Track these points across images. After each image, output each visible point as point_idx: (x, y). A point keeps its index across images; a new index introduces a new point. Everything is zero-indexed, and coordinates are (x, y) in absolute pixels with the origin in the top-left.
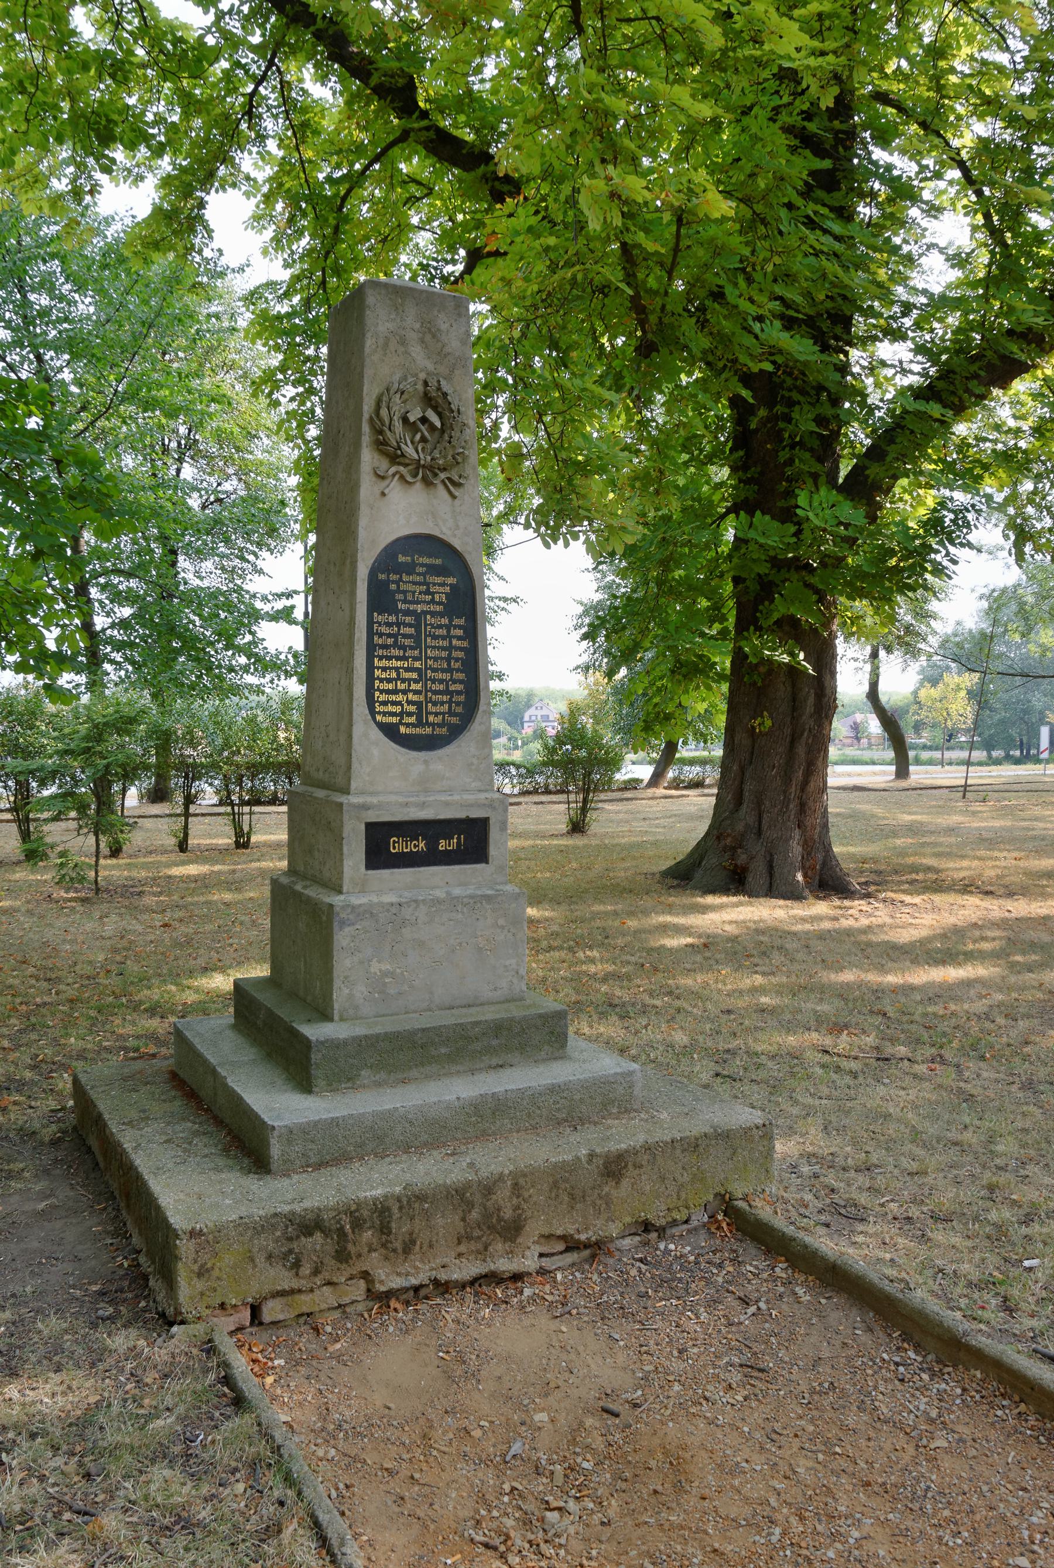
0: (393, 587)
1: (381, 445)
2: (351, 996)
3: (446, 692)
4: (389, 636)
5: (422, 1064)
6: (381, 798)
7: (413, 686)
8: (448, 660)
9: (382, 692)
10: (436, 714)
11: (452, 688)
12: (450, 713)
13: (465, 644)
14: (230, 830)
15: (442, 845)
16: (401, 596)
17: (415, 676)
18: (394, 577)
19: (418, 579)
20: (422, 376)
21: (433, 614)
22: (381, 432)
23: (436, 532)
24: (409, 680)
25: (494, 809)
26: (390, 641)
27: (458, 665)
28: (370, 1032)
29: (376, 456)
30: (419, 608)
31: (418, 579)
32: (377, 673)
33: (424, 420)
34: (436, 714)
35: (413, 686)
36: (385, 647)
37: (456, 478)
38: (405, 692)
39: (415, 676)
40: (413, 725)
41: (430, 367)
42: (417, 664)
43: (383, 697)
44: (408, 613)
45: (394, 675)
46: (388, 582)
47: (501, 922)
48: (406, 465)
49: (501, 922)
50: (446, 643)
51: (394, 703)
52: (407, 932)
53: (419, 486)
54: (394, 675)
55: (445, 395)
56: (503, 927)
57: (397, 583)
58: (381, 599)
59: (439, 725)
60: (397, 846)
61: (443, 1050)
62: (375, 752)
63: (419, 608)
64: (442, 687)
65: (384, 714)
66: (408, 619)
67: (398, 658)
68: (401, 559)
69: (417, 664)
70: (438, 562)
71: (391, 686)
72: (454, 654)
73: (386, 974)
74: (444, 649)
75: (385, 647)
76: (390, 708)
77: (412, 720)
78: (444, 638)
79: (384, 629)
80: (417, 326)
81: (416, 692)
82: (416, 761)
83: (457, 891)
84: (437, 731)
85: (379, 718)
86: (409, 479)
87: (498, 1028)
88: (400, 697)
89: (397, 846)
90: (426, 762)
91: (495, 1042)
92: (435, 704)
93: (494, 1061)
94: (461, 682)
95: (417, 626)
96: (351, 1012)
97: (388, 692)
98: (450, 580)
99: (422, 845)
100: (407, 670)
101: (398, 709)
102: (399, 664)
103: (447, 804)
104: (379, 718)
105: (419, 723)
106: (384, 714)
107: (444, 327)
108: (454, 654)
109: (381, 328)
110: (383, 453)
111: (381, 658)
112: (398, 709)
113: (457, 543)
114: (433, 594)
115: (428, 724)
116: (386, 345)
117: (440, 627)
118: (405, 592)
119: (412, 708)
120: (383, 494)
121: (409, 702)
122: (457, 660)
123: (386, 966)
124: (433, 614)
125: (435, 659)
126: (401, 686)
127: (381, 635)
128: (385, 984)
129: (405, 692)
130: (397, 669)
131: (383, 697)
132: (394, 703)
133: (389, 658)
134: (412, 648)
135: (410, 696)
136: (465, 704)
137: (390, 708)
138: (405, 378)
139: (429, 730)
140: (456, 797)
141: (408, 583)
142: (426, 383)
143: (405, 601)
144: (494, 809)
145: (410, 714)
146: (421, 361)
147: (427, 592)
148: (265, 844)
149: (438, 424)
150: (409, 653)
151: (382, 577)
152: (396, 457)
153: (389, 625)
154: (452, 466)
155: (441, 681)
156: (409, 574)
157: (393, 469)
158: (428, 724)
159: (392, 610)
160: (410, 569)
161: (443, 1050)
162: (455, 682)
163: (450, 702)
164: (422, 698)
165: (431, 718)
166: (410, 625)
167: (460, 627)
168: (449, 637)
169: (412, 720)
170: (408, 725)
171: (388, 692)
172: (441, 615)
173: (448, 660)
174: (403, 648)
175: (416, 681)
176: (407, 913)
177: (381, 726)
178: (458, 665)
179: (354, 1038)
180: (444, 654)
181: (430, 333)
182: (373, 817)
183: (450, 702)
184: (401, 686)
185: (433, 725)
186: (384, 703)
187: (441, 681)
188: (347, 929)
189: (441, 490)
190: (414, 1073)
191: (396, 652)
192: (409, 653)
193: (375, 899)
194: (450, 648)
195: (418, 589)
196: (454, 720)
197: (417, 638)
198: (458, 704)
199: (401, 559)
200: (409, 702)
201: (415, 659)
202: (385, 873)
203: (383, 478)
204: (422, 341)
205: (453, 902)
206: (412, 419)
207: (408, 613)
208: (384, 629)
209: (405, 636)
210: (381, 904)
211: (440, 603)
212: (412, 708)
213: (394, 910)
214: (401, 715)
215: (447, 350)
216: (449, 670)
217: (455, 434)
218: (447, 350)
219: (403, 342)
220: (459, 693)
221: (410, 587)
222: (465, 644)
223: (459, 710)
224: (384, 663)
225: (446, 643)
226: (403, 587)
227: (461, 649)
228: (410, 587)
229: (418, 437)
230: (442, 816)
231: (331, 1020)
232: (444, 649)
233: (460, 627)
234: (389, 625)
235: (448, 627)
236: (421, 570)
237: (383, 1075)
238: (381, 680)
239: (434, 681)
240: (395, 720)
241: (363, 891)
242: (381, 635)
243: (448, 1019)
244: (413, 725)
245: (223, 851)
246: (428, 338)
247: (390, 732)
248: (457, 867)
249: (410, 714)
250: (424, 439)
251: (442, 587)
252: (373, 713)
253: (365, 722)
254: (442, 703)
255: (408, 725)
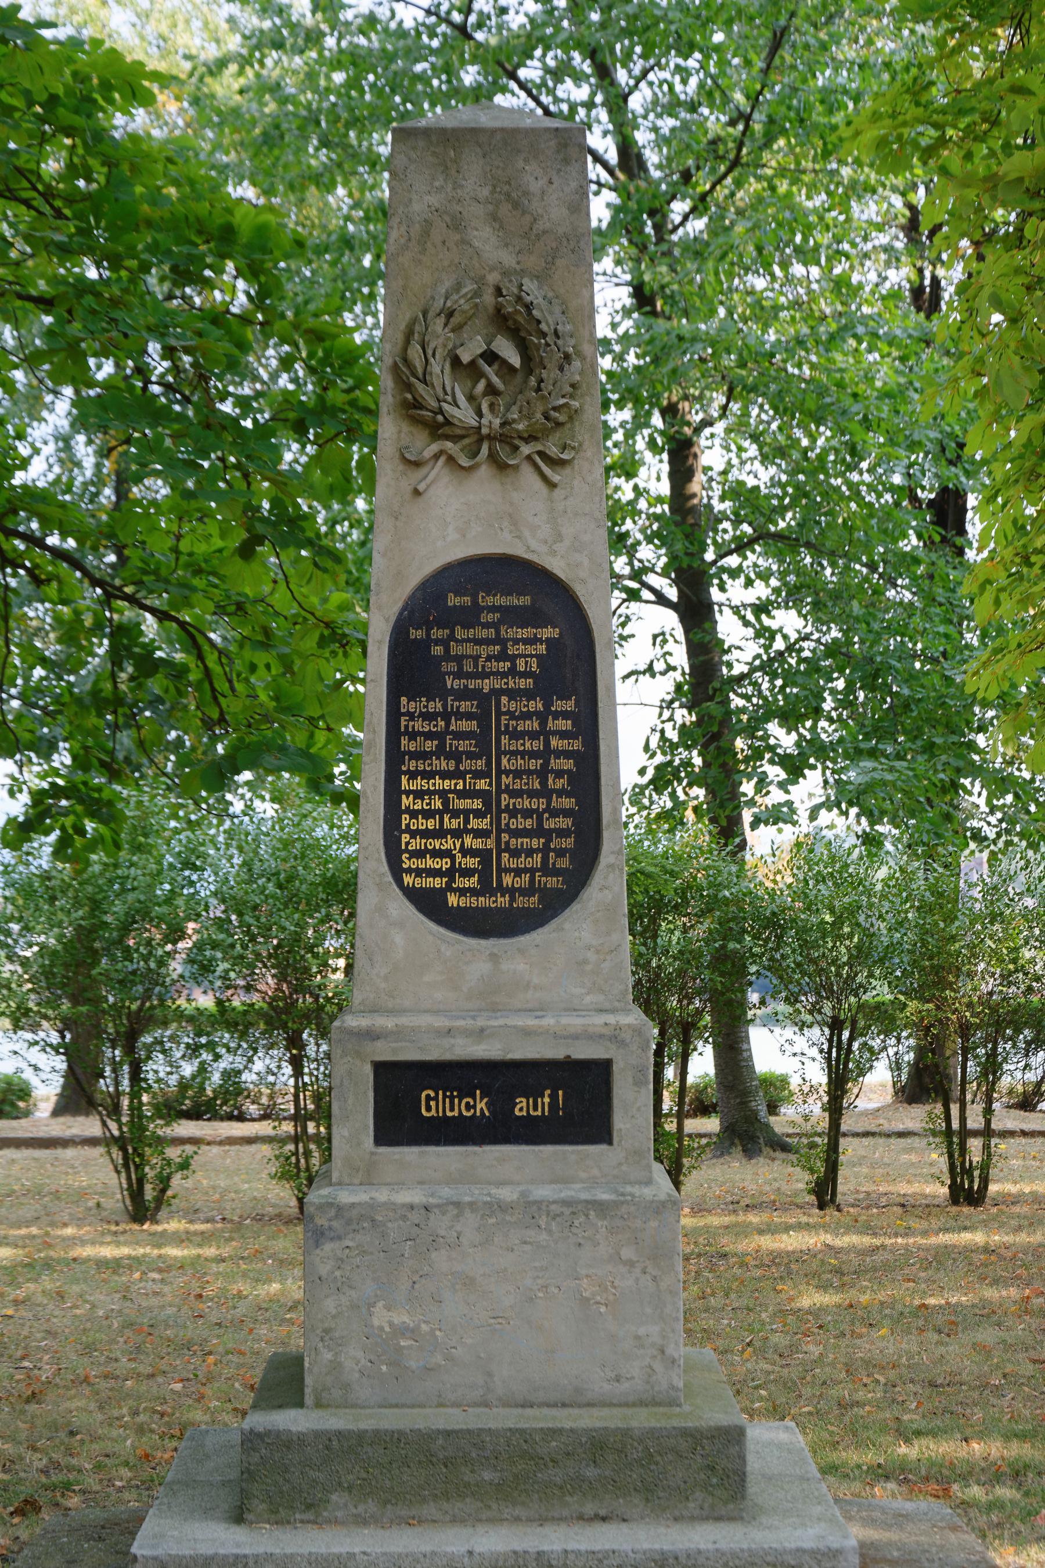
0: (438, 650)
1: (411, 408)
2: (336, 1366)
3: (539, 831)
4: (429, 736)
5: (446, 1496)
6: (404, 1021)
7: (474, 823)
8: (543, 773)
9: (414, 834)
10: (518, 872)
11: (550, 824)
12: (546, 870)
13: (577, 745)
14: (938, 1159)
15: (521, 1107)
16: (452, 666)
17: (477, 804)
18: (437, 633)
19: (483, 633)
20: (493, 278)
21: (513, 694)
22: (409, 387)
23: (518, 550)
24: (466, 813)
25: (622, 1044)
26: (430, 745)
27: (561, 783)
28: (351, 1427)
29: (405, 427)
30: (486, 685)
31: (483, 633)
32: (406, 801)
33: (490, 357)
34: (518, 872)
35: (474, 823)
36: (421, 755)
37: (553, 451)
38: (457, 834)
39: (477, 804)
40: (473, 892)
41: (509, 260)
42: (482, 784)
43: (416, 844)
44: (464, 694)
45: (438, 804)
46: (426, 644)
47: (627, 1253)
48: (455, 439)
49: (627, 1253)
50: (537, 745)
51: (437, 854)
52: (440, 1259)
53: (485, 471)
54: (438, 804)
55: (529, 307)
56: (631, 1264)
57: (445, 643)
58: (412, 670)
59: (525, 892)
60: (434, 1105)
61: (487, 1476)
62: (398, 938)
63: (486, 685)
64: (529, 823)
65: (419, 872)
66: (465, 706)
67: (445, 775)
68: (453, 600)
69: (482, 784)
70: (525, 601)
71: (431, 824)
72: (555, 764)
73: (402, 1331)
74: (533, 755)
75: (421, 755)
76: (430, 863)
77: (473, 882)
78: (533, 735)
79: (419, 725)
80: (485, 192)
81: (478, 834)
82: (477, 957)
83: (543, 1192)
84: (520, 902)
85: (408, 880)
86: (464, 462)
87: (598, 1446)
88: (448, 843)
89: (434, 1105)
90: (494, 957)
91: (590, 1472)
92: (515, 853)
93: (589, 1509)
94: (566, 813)
95: (483, 718)
96: (336, 1393)
97: (426, 834)
98: (548, 633)
99: (481, 1105)
100: (463, 794)
101: (445, 864)
102: (447, 784)
103: (527, 1033)
104: (408, 880)
105: (486, 888)
106: (419, 872)
107: (535, 187)
108: (555, 764)
109: (416, 207)
110: (416, 421)
111: (413, 775)
112: (445, 864)
113: (557, 566)
114: (513, 659)
115: (502, 890)
116: (426, 233)
117: (527, 716)
118: (459, 659)
119: (472, 862)
120: (417, 493)
121: (465, 852)
122: (559, 774)
123: (401, 1318)
124: (513, 694)
125: (517, 774)
126: (451, 823)
127: (413, 736)
128: (399, 1349)
129: (457, 834)
130: (443, 794)
131: (416, 844)
132: (437, 854)
133: (428, 775)
134: (471, 756)
135: (468, 841)
136: (573, 853)
137: (430, 863)
138: (458, 287)
139: (503, 901)
140: (549, 1021)
141: (466, 643)
142: (498, 291)
143: (459, 675)
144: (622, 1044)
145: (467, 873)
146: (491, 250)
147: (503, 656)
148: (1015, 1200)
149: (515, 361)
150: (466, 765)
151: (416, 634)
152: (439, 427)
153: (428, 717)
154: (546, 433)
155: (527, 813)
156: (466, 626)
157: (435, 447)
158: (502, 890)
159: (434, 689)
160: (469, 617)
161: (487, 1476)
162: (554, 813)
163: (545, 850)
164: (491, 843)
165: (508, 880)
166: (469, 716)
167: (565, 715)
168: (544, 733)
169: (473, 882)
170: (462, 892)
171: (426, 834)
172: (529, 694)
173: (543, 773)
174: (456, 756)
175: (479, 814)
176: (440, 1224)
177: (414, 895)
178: (561, 783)
179: (317, 1434)
180: (534, 764)
181: (509, 202)
182: (386, 1052)
183: (545, 850)
184: (451, 823)
185: (512, 891)
186: (419, 854)
187: (527, 813)
188: (328, 1247)
189: (528, 476)
190: (430, 1510)
191: (443, 765)
192: (466, 765)
193: (382, 1195)
194: (547, 753)
195: (484, 651)
196: (552, 882)
197: (482, 739)
198: (561, 853)
199: (453, 600)
200: (465, 852)
201: (478, 775)
202: (410, 1153)
203: (417, 464)
204: (494, 217)
205: (532, 1210)
206: (466, 358)
207: (464, 694)
208: (419, 725)
209: (459, 735)
210: (391, 1206)
211: (525, 675)
212: (472, 862)
213: (415, 1217)
214: (450, 874)
215: (540, 226)
216: (545, 793)
217: (550, 374)
218: (540, 226)
219: (457, 224)
220: (562, 833)
221: (470, 649)
222: (577, 745)
223: (564, 863)
224: (419, 784)
225: (537, 745)
226: (455, 649)
227: (567, 754)
228: (470, 649)
229: (481, 386)
230: (517, 1055)
231: (301, 1404)
232: (533, 755)
233: (565, 715)
234: (428, 717)
235: (542, 717)
236: (490, 617)
237: (371, 1507)
238: (414, 814)
239: (513, 813)
240: (438, 883)
241: (368, 1182)
242: (413, 736)
243: (502, 1419)
244: (473, 892)
245: (928, 1208)
246: (505, 209)
247: (430, 904)
248: (548, 1149)
249: (467, 873)
250: (491, 390)
251: (531, 646)
252: (397, 871)
253: (381, 887)
254: (530, 852)
255: (462, 892)
